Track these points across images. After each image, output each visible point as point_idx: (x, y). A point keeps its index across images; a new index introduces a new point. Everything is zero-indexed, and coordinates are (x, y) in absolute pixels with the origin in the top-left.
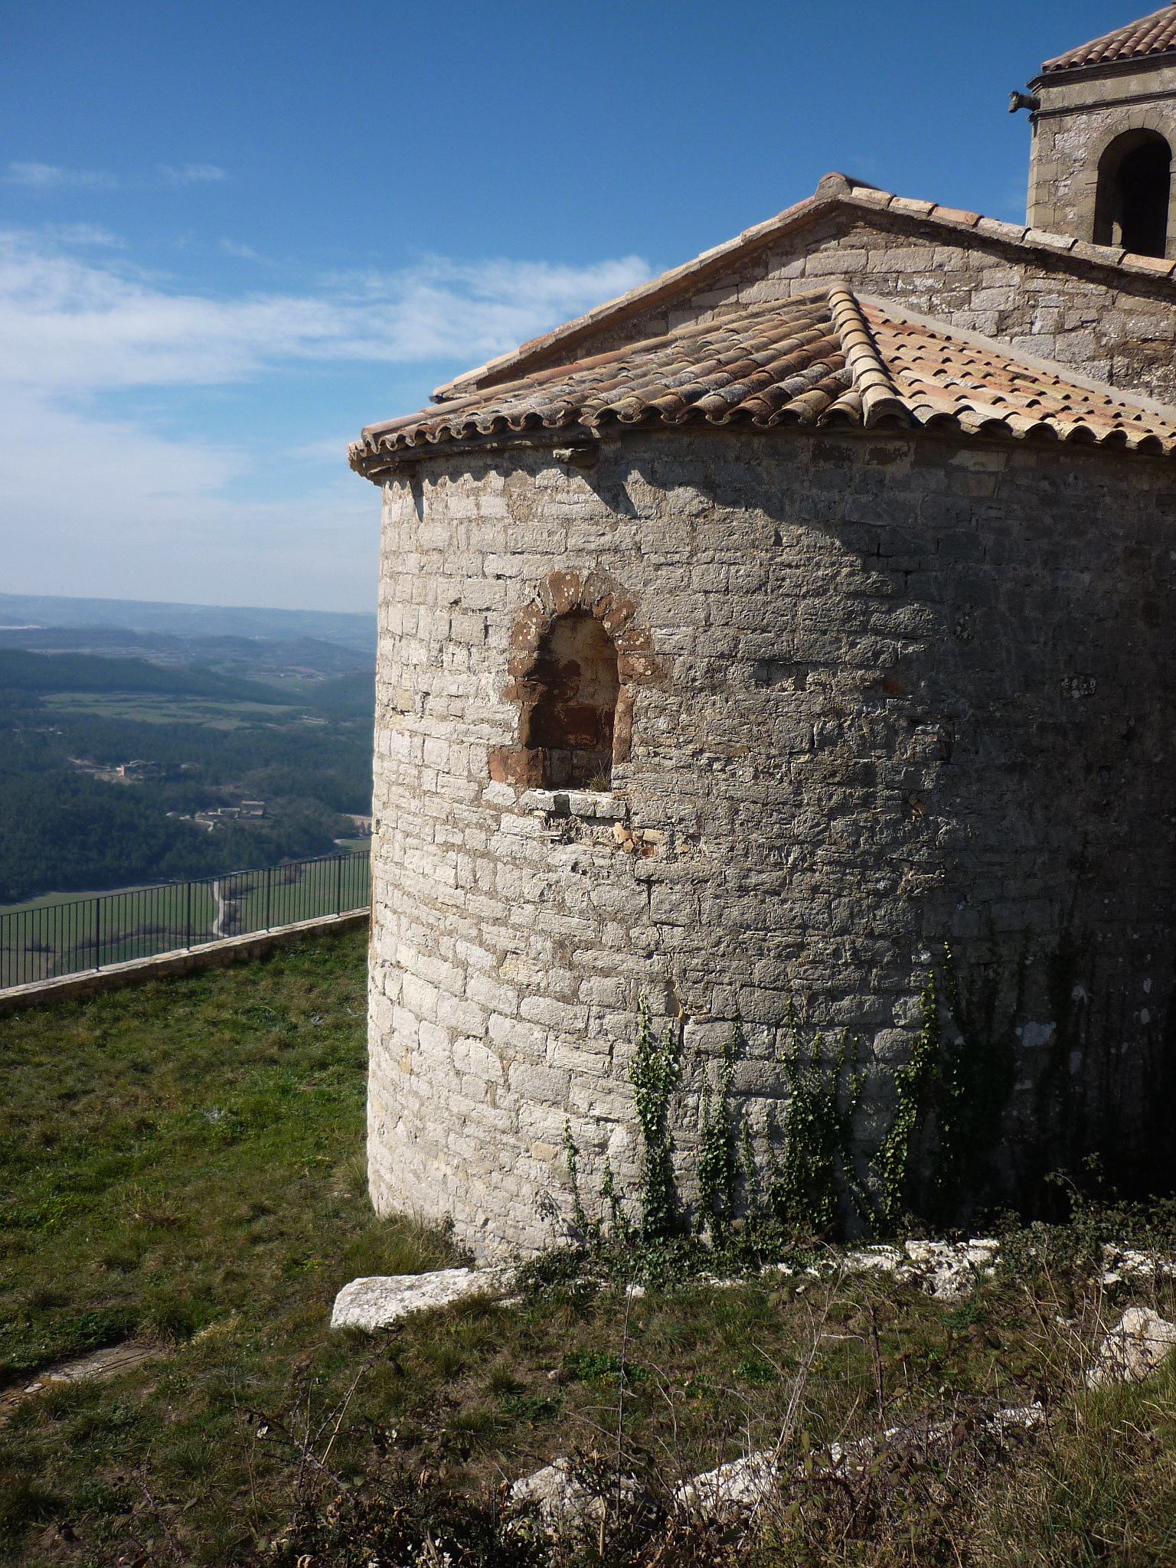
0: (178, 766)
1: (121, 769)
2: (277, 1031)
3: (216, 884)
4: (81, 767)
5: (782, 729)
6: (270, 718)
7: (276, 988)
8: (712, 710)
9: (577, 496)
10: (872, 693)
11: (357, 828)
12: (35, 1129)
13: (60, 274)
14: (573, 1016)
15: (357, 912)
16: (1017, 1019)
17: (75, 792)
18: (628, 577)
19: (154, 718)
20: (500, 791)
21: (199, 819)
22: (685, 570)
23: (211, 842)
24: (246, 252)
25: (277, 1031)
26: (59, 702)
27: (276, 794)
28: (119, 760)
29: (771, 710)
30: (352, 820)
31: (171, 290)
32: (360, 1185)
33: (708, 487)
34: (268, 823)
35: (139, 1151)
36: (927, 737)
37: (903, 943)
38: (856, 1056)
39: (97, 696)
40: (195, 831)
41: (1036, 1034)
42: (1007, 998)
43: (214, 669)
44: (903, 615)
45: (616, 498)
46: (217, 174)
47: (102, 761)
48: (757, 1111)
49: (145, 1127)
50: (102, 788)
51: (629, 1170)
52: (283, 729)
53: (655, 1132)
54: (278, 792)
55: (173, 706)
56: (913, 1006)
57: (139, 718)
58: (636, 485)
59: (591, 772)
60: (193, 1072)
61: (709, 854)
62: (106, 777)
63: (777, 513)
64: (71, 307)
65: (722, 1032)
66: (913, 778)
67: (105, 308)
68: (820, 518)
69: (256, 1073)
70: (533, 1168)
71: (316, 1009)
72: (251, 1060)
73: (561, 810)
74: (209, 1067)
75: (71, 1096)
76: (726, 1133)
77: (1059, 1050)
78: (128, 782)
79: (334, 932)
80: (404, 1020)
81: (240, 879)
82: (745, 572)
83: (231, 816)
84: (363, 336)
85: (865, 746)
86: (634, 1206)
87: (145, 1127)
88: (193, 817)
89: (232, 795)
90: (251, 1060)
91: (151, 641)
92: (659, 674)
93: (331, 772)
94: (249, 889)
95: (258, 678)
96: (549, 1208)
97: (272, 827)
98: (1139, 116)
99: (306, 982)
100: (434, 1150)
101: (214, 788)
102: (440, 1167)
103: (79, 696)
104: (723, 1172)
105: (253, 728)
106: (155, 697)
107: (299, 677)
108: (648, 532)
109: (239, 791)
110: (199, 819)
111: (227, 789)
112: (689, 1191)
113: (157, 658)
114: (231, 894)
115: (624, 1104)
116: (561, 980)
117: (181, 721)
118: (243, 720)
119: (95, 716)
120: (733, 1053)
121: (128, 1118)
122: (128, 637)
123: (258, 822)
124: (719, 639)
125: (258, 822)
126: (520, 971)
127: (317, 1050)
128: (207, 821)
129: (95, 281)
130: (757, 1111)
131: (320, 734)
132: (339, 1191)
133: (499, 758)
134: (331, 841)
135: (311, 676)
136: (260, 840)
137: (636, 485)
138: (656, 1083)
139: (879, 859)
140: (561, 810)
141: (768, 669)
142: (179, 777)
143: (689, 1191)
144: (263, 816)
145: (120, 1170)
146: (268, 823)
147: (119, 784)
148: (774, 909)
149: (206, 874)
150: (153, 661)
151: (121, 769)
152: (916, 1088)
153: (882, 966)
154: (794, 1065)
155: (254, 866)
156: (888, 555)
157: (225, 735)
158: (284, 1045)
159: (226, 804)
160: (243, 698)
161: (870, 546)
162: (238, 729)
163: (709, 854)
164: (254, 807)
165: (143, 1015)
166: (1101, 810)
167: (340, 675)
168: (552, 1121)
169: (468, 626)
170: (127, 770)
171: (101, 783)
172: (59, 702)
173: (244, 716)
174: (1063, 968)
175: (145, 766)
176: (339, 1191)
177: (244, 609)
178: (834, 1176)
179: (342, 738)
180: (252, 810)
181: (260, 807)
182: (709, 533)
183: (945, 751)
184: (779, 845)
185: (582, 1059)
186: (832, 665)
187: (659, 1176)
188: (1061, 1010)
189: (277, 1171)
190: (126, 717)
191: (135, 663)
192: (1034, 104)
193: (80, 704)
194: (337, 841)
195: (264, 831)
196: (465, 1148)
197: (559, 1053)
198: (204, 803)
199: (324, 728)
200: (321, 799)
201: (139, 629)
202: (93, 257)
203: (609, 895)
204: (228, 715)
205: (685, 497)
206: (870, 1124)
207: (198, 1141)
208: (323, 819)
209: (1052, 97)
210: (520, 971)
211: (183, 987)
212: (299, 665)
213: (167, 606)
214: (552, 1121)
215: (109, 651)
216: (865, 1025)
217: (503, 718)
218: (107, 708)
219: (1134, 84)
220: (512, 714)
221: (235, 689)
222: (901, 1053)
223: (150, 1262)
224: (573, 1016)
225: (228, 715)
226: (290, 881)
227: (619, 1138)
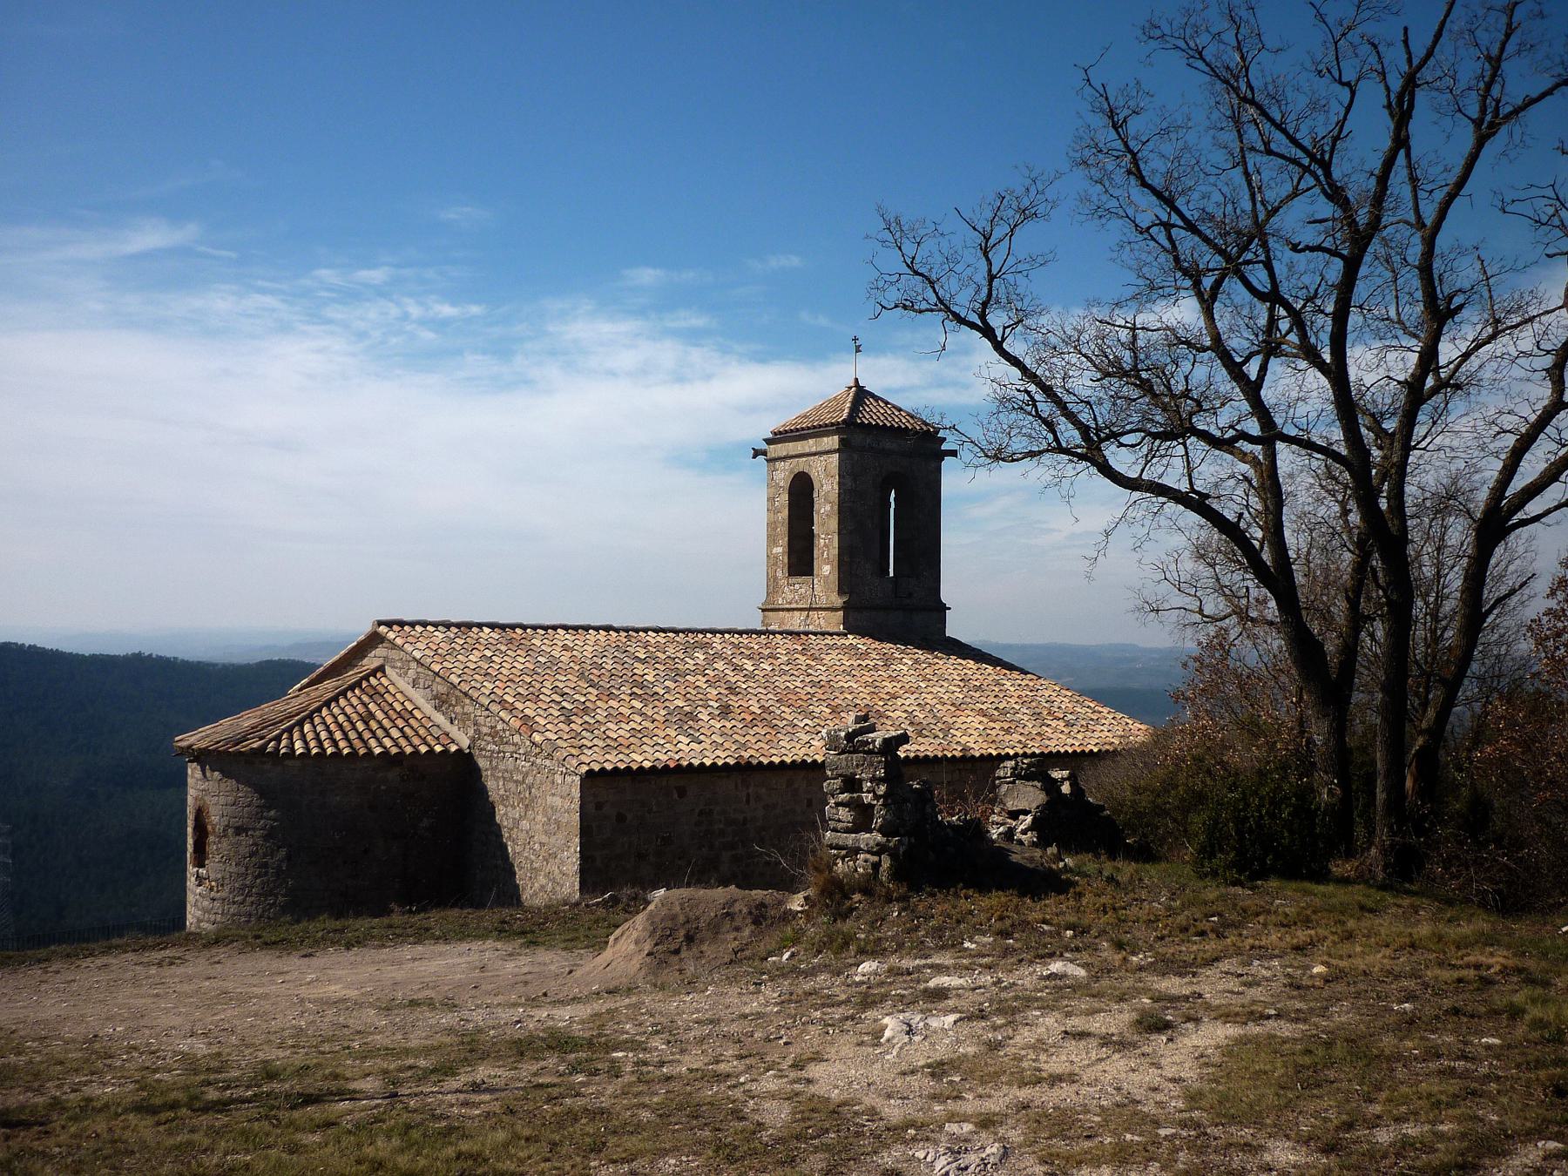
10: (266, 838)
13: (667, 353)
24: (823, 321)
29: (239, 844)
31: (761, 358)
33: (222, 771)
36: (283, 852)
44: (272, 813)
46: (795, 261)
63: (238, 782)
64: (679, 378)
66: (279, 866)
67: (708, 377)
68: (248, 783)
82: (230, 799)
84: (941, 383)
85: (265, 855)
98: (801, 465)
124: (225, 821)
129: (696, 355)
139: (271, 893)
141: (239, 830)
156: (268, 795)
161: (261, 791)
182: (223, 785)
183: (289, 857)
186: (254, 829)
202: (693, 337)
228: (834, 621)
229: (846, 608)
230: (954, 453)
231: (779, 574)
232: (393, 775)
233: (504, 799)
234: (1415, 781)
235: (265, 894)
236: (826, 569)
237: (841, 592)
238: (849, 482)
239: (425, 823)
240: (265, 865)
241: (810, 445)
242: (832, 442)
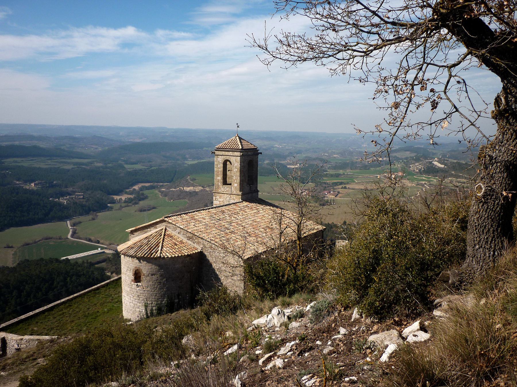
0: (53, 182)
1: (33, 184)
2: (111, 298)
3: (68, 222)
4: (18, 184)
5: (153, 279)
6: (83, 164)
7: (110, 291)
8: (148, 278)
9: (137, 261)
10: (160, 276)
11: (115, 200)
12: (87, 313)
14: (139, 301)
15: (120, 276)
16: (175, 299)
17: (17, 193)
18: (141, 268)
19: (43, 166)
20: (133, 283)
21: (61, 200)
22: (145, 268)
23: (66, 208)
25: (111, 298)
26: (9, 162)
27: (87, 190)
28: (32, 181)
29: (153, 278)
30: (113, 198)
32: (122, 316)
34: (85, 200)
35: (98, 314)
37: (164, 294)
38: (161, 303)
39: (23, 159)
40: (60, 204)
41: (176, 301)
42: (174, 298)
43: (62, 148)
45: (140, 261)
47: (26, 182)
48: (154, 308)
49: (98, 312)
50: (26, 191)
51: (144, 313)
52: (88, 168)
53: (146, 310)
54: (88, 189)
55: (49, 161)
56: (166, 299)
57: (38, 166)
58: (141, 261)
59: (139, 282)
60: (102, 304)
61: (149, 289)
62: (27, 187)
65: (151, 302)
69: (109, 304)
70: (137, 314)
71: (115, 294)
72: (108, 302)
73: (137, 285)
74: (103, 304)
75: (88, 309)
76: (152, 310)
77: (179, 302)
78: (35, 188)
79: (116, 280)
80: (126, 301)
81: (76, 219)
83: (72, 198)
86: (145, 316)
87: (98, 312)
88: (59, 199)
89: (72, 191)
90: (108, 302)
91: (40, 138)
92: (144, 275)
93: (105, 182)
94: (80, 223)
95: (79, 150)
96: (138, 317)
97: (86, 201)
98: (227, 158)
99: (113, 290)
100: (129, 313)
101: (65, 189)
102: (130, 314)
103: (15, 159)
104: (152, 313)
105: (78, 168)
106: (43, 158)
107: (92, 149)
108: (142, 264)
109: (74, 190)
110: (61, 200)
111: (70, 189)
112: (149, 315)
113: (42, 145)
114: (74, 225)
115: (144, 308)
116: (138, 298)
117: (53, 166)
118: (74, 165)
119: (22, 166)
120: (152, 304)
121: (96, 311)
122: (32, 138)
123: (82, 200)
124: (148, 273)
125: (82, 200)
126: (135, 298)
127: (116, 300)
128: (64, 201)
130: (154, 308)
131: (101, 169)
132: (120, 317)
133: (132, 280)
134: (107, 205)
135: (96, 149)
136: (82, 206)
137: (141, 261)
138: (146, 306)
140: (137, 285)
141: (152, 275)
142: (52, 186)
143: (149, 315)
144: (83, 198)
145: (97, 316)
146: (85, 200)
147: (33, 190)
148: (154, 293)
149: (63, 218)
150: (41, 146)
151: (33, 184)
152: (167, 306)
153: (163, 296)
154: (157, 304)
155: (81, 214)
156: (161, 267)
157: (68, 170)
158: (112, 300)
159: (70, 195)
160: (73, 158)
162: (73, 168)
163: (149, 289)
164: (81, 195)
165: (93, 297)
166: (181, 282)
167: (107, 148)
168: (138, 310)
169: (129, 269)
170: (35, 184)
171: (26, 190)
172: (9, 162)
173: (75, 164)
174: (178, 295)
175: (41, 183)
176: (120, 317)
177: (72, 126)
178: (160, 311)
179: (109, 170)
180: (79, 195)
181: (81, 195)
183: (167, 280)
184: (154, 288)
185: (140, 305)
187: (147, 314)
188: (178, 298)
189: (114, 315)
190: (33, 166)
191: (35, 147)
192: (214, 153)
193: (16, 162)
194: (109, 205)
195: (84, 203)
196: (131, 312)
197: (138, 304)
198: (63, 195)
199: (102, 167)
200: (102, 191)
201: (35, 134)
203: (141, 292)
204: (69, 163)
205: (145, 262)
206: (163, 309)
207: (104, 313)
208: (103, 198)
209: (217, 153)
210: (135, 298)
211: (97, 292)
212: (92, 145)
213: (45, 125)
214: (138, 310)
215: (27, 143)
216: (162, 301)
217: (133, 277)
218: (26, 163)
219: (227, 153)
220: (133, 277)
221: (71, 155)
222: (165, 303)
223: (104, 324)
224: (139, 301)
225: (69, 163)
226: (93, 219)
227: (143, 311)
228: (238, 199)
229: (242, 195)
230: (261, 153)
231: (220, 184)
232: (188, 259)
233: (214, 262)
234: (192, 165)
235: (160, 289)
236: (236, 185)
237: (240, 191)
238: (242, 164)
239: (194, 268)
240: (160, 282)
241: (230, 153)
242: (238, 154)
